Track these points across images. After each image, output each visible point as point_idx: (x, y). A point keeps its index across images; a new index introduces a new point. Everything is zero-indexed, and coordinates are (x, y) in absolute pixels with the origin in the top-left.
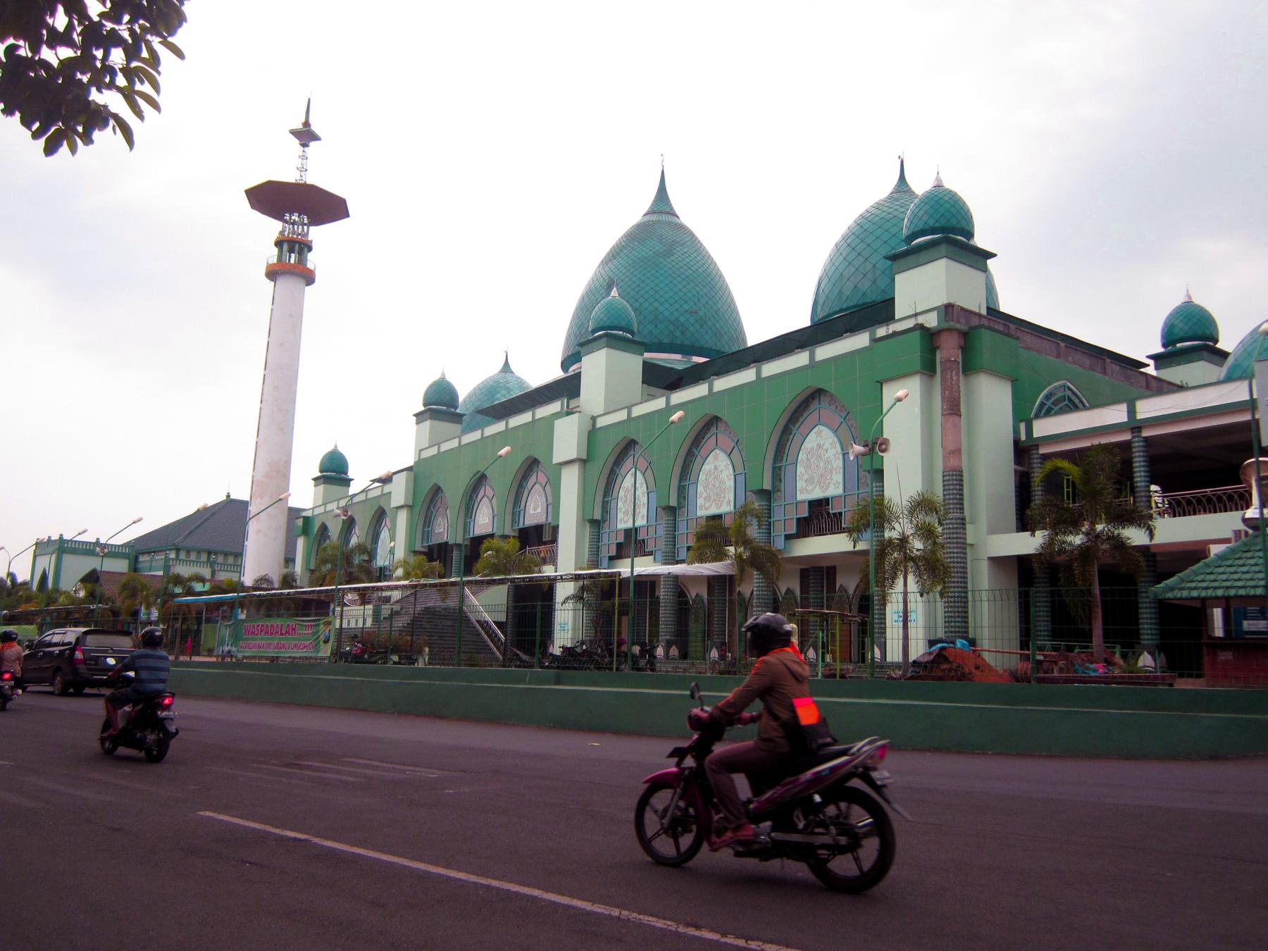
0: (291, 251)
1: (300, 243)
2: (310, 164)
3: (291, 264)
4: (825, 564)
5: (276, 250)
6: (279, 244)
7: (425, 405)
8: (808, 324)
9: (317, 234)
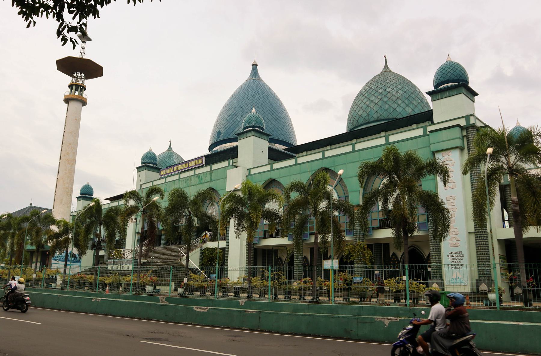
0: (76, 90)
1: (81, 86)
2: (85, 51)
3: (76, 97)
4: (274, 248)
5: (69, 90)
6: (71, 86)
7: (142, 163)
8: (345, 131)
9: (88, 83)
